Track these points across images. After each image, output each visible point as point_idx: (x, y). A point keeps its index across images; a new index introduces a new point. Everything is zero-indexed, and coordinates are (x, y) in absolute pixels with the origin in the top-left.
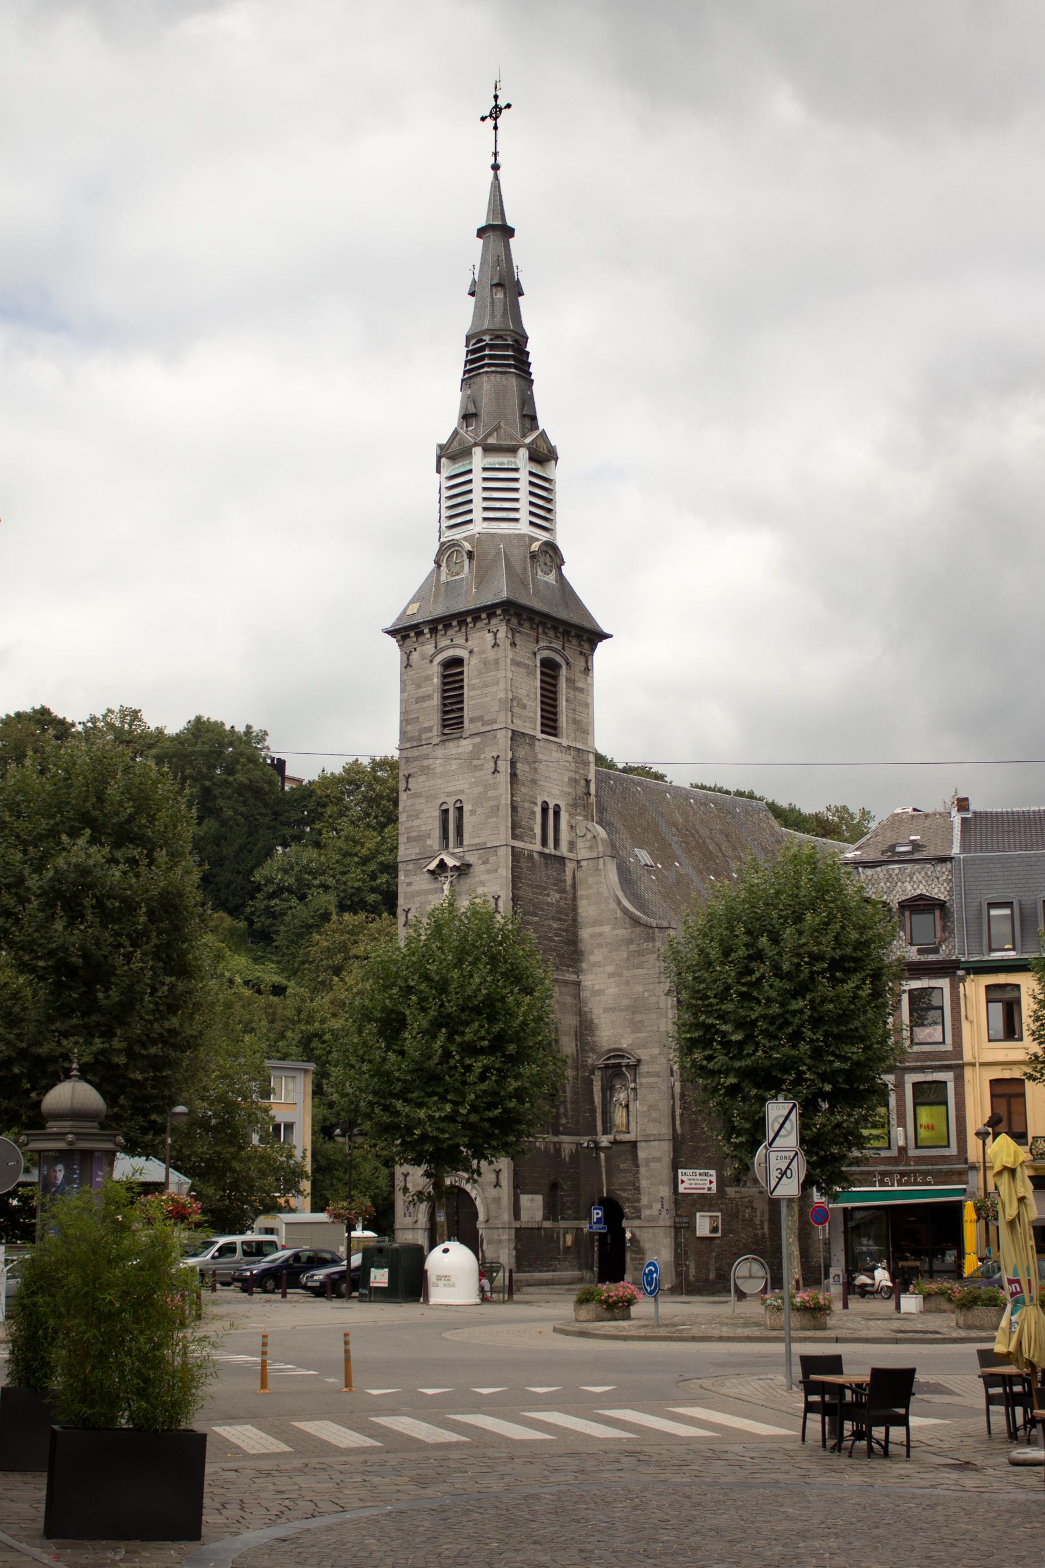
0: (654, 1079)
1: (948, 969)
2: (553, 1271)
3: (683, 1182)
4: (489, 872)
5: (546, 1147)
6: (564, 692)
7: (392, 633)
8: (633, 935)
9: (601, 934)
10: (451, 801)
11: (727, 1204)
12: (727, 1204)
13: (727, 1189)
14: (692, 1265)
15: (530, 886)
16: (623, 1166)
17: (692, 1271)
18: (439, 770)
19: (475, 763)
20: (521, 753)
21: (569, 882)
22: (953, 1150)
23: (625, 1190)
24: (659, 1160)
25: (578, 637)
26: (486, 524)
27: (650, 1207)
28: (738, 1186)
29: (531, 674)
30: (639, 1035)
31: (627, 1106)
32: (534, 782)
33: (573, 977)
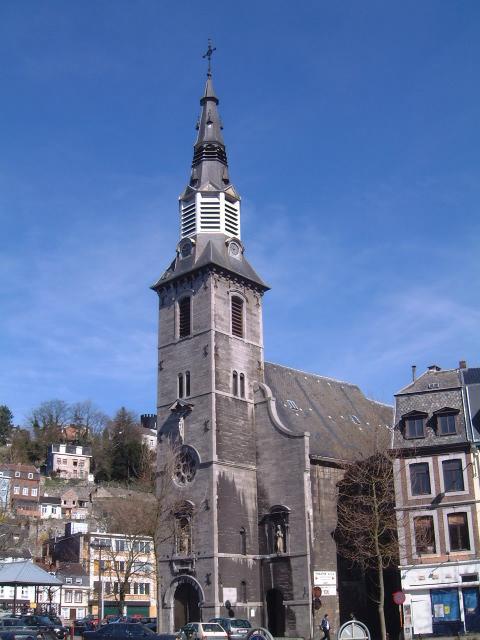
4: (203, 408)
7: (154, 288)
9: (268, 443)
16: (283, 571)
20: (221, 344)
29: (226, 302)
32: (228, 360)
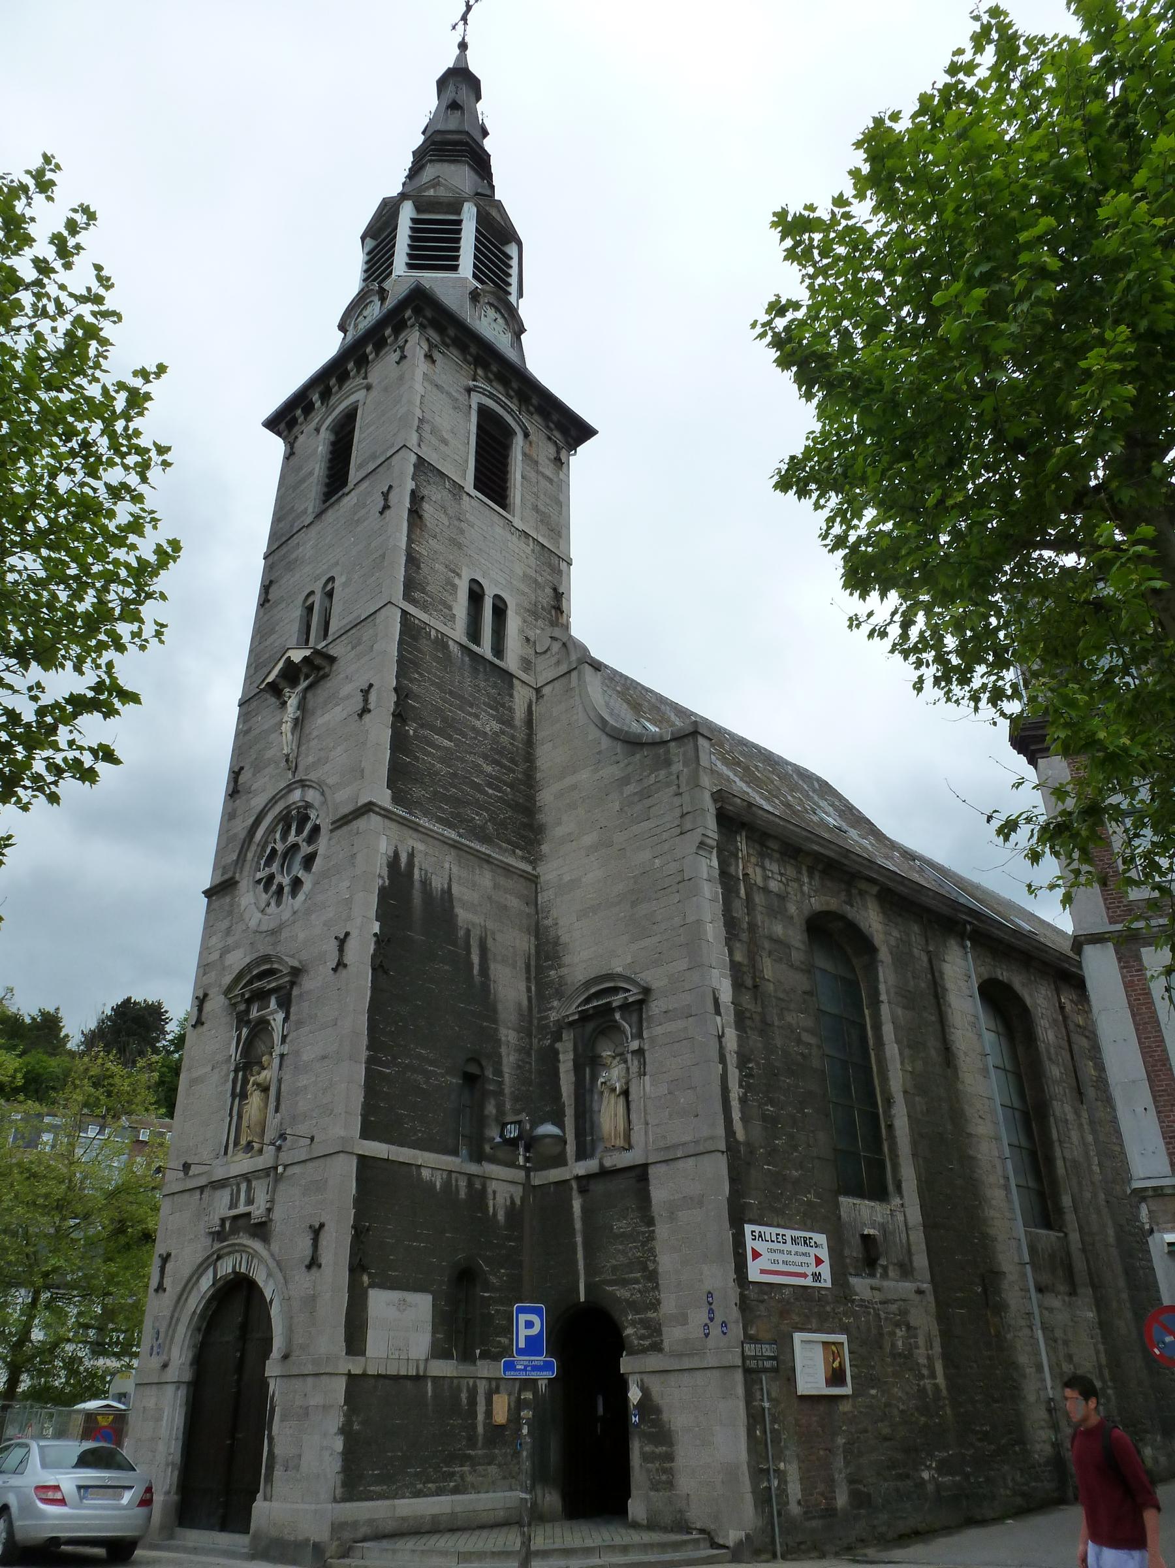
0: (680, 1024)
2: (456, 1491)
3: (756, 1255)
5: (447, 1184)
8: (630, 769)
11: (855, 1315)
13: (853, 1280)
14: (792, 1470)
17: (794, 1489)
23: (624, 1283)
24: (700, 1202)
27: (683, 1319)
28: (872, 1275)
31: (626, 1093)
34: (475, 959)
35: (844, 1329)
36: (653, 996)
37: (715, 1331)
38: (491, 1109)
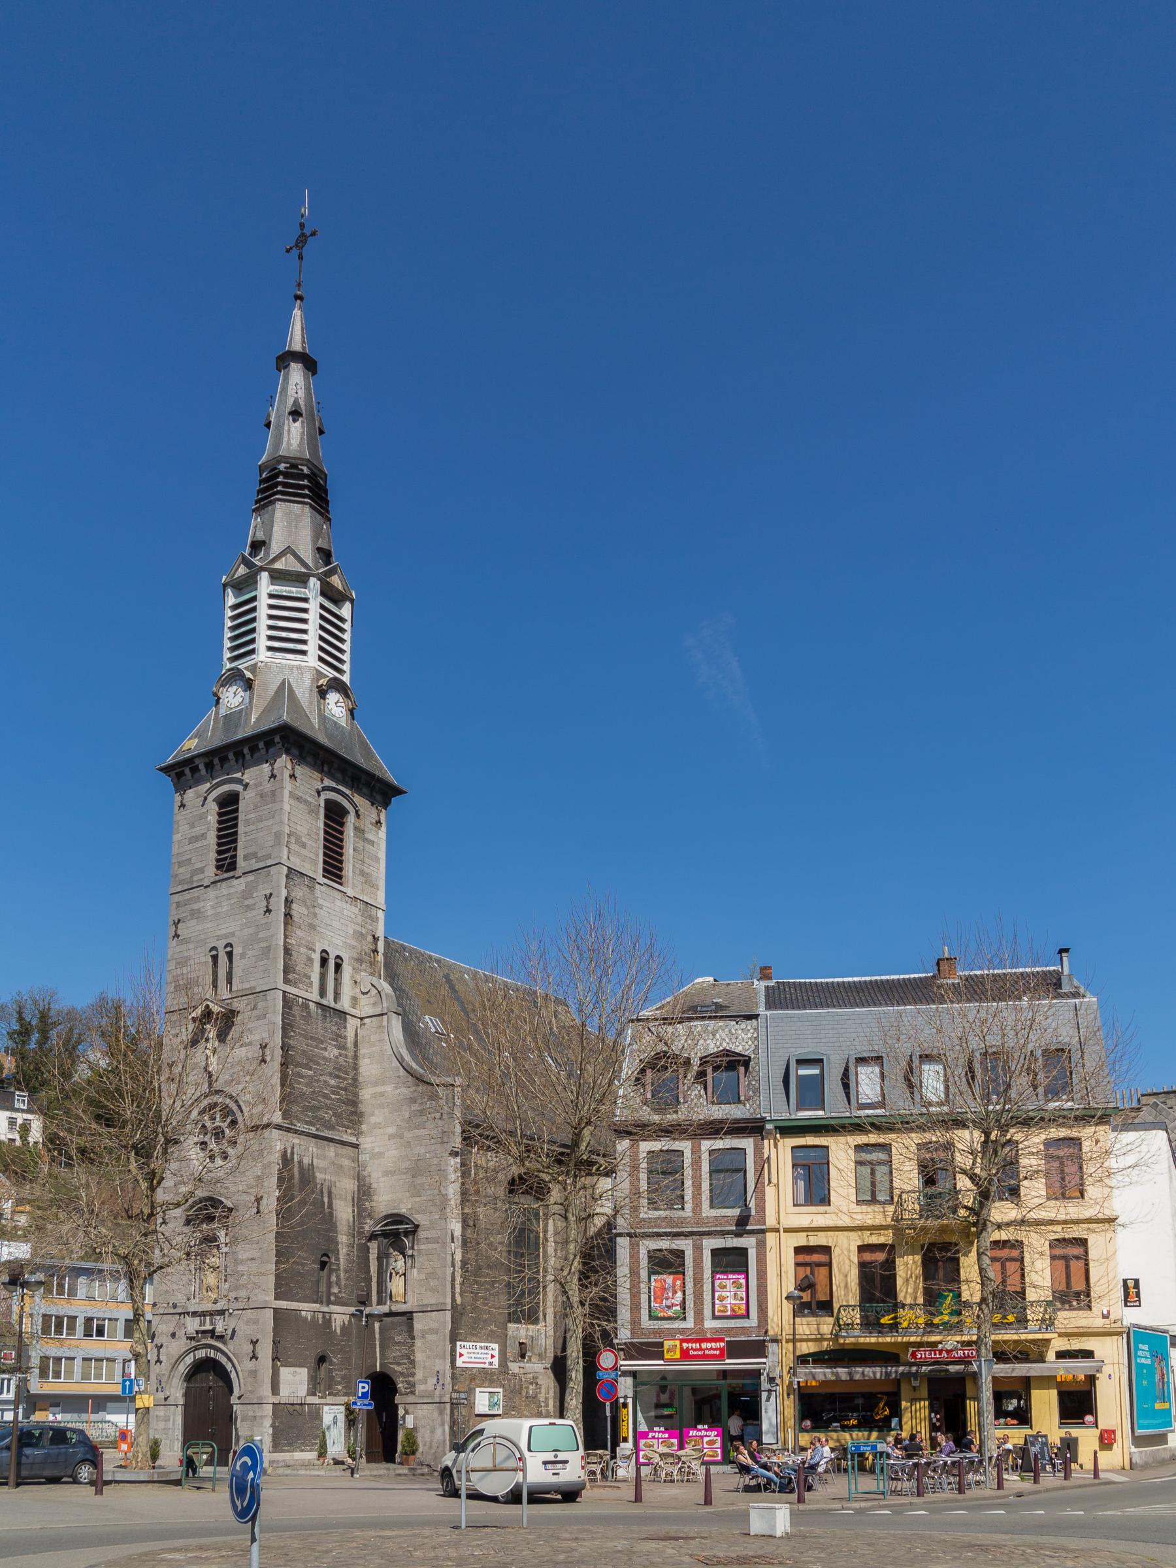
1: (754, 1128)
3: (461, 1355)
5: (313, 1317)
6: (352, 839)
7: (166, 770)
9: (382, 1094)
10: (220, 945)
11: (509, 1380)
12: (509, 1380)
15: (305, 1037)
16: (398, 1338)
18: (209, 913)
19: (247, 902)
21: (350, 1045)
22: (754, 1321)
23: (399, 1364)
25: (368, 785)
26: (269, 654)
27: (425, 1382)
29: (313, 811)
30: (418, 1199)
31: (404, 1274)
32: (312, 927)
33: (353, 1139)
34: (326, 1200)
35: (502, 1386)
36: (420, 1229)
37: (439, 1388)
38: (334, 1278)
